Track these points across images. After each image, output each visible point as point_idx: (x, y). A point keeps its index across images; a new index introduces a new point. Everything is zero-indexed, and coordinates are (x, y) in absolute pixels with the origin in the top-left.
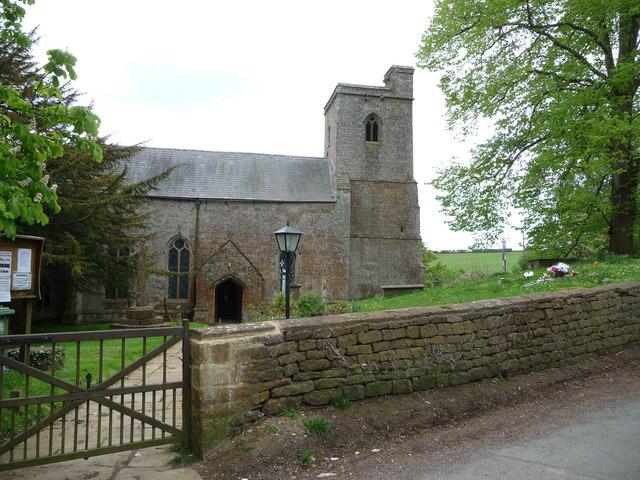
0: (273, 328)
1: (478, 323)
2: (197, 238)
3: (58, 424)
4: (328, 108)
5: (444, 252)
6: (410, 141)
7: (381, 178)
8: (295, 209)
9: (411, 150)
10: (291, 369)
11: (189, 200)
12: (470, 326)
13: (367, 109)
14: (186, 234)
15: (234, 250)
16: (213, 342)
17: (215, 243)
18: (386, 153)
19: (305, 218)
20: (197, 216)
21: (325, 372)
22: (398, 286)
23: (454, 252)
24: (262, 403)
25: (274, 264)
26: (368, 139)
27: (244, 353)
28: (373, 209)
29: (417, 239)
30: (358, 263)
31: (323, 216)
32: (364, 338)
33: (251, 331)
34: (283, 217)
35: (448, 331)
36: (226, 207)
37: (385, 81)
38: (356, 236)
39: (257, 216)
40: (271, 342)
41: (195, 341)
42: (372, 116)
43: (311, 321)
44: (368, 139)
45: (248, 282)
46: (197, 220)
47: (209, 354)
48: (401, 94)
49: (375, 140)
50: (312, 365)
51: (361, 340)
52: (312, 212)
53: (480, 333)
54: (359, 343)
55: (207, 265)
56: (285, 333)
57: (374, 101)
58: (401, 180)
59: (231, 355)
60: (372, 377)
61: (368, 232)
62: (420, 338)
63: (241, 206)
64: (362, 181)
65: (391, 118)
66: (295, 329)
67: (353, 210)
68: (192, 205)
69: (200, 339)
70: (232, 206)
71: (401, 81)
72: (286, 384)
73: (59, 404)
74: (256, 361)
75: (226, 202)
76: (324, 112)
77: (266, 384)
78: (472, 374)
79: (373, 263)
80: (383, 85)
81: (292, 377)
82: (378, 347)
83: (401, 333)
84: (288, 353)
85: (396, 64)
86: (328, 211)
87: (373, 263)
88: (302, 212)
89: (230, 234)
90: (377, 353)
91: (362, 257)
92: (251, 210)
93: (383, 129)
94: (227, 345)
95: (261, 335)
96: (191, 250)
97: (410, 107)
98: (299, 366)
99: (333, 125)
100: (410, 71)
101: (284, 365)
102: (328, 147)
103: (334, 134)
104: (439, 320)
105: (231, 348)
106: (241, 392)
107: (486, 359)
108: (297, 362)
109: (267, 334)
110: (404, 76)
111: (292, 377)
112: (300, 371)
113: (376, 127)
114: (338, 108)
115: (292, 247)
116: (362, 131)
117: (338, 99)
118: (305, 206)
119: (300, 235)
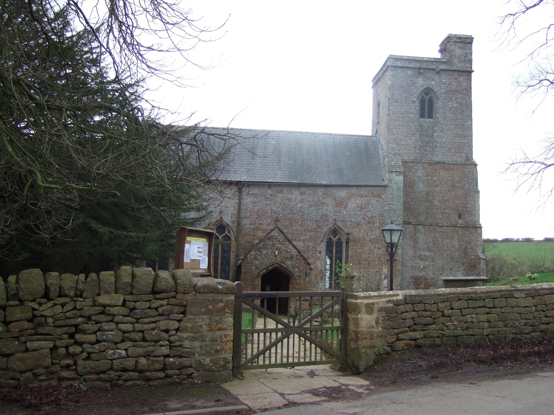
0: (398, 295)
1: (537, 300)
2: (239, 224)
3: (279, 344)
4: (377, 80)
5: (506, 241)
6: (469, 117)
7: (436, 159)
8: (342, 193)
9: (470, 128)
10: (409, 322)
11: (231, 183)
12: (530, 301)
13: (421, 83)
14: (228, 220)
15: (281, 238)
16: (366, 301)
17: (257, 229)
18: (442, 131)
19: (353, 204)
20: (240, 200)
21: (431, 326)
22: (455, 278)
23: (518, 241)
24: (392, 343)
25: (320, 252)
26: (422, 116)
27: (380, 310)
28: (428, 193)
29: (477, 228)
30: (411, 253)
31: (374, 201)
32: (456, 305)
33: (386, 296)
34: (330, 201)
35: (514, 304)
36: (270, 191)
37: (441, 51)
38: (409, 223)
39: (302, 201)
40: (397, 304)
41: (349, 300)
42: (428, 91)
43: (421, 292)
44: (422, 116)
45: (296, 272)
46: (240, 204)
47: (363, 309)
48: (459, 66)
49: (430, 116)
50: (422, 321)
51: (453, 306)
52: (362, 196)
53: (539, 308)
54: (452, 309)
55: (253, 253)
56: (405, 298)
57: (430, 74)
58: (459, 160)
59: (376, 310)
60: (460, 332)
61: (422, 218)
62: (494, 307)
63: (285, 190)
64: (415, 162)
65: (447, 92)
66: (411, 296)
67: (406, 194)
68: (235, 188)
69: (357, 299)
70: (275, 189)
71: (458, 52)
72: (406, 332)
73: (280, 334)
74: (389, 315)
75: (270, 185)
76: (371, 84)
77: (395, 330)
78: (532, 337)
79: (427, 253)
80: (438, 56)
81: (409, 327)
82: (465, 312)
83: (481, 303)
84: (407, 312)
85: (454, 32)
86: (379, 196)
87: (427, 253)
88: (350, 197)
89: (277, 220)
90: (464, 316)
91: (415, 247)
92: (295, 195)
93: (439, 104)
94: (373, 304)
95: (391, 299)
96: (232, 236)
97: (470, 80)
98: (414, 320)
99: (384, 101)
100: (468, 41)
101: (405, 319)
102: (377, 123)
103: (384, 111)
104: (509, 295)
105: (376, 306)
106: (380, 334)
107: (543, 327)
108: (413, 318)
109: (395, 298)
110: (462, 45)
111: (409, 327)
112: (415, 324)
113: (431, 102)
114: (389, 82)
115: (395, 239)
116: (415, 108)
117: (389, 73)
118: (354, 190)
119: (401, 230)
